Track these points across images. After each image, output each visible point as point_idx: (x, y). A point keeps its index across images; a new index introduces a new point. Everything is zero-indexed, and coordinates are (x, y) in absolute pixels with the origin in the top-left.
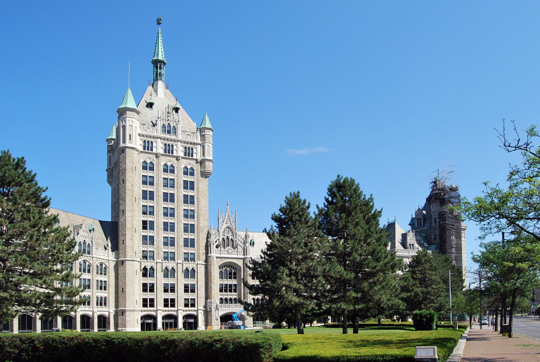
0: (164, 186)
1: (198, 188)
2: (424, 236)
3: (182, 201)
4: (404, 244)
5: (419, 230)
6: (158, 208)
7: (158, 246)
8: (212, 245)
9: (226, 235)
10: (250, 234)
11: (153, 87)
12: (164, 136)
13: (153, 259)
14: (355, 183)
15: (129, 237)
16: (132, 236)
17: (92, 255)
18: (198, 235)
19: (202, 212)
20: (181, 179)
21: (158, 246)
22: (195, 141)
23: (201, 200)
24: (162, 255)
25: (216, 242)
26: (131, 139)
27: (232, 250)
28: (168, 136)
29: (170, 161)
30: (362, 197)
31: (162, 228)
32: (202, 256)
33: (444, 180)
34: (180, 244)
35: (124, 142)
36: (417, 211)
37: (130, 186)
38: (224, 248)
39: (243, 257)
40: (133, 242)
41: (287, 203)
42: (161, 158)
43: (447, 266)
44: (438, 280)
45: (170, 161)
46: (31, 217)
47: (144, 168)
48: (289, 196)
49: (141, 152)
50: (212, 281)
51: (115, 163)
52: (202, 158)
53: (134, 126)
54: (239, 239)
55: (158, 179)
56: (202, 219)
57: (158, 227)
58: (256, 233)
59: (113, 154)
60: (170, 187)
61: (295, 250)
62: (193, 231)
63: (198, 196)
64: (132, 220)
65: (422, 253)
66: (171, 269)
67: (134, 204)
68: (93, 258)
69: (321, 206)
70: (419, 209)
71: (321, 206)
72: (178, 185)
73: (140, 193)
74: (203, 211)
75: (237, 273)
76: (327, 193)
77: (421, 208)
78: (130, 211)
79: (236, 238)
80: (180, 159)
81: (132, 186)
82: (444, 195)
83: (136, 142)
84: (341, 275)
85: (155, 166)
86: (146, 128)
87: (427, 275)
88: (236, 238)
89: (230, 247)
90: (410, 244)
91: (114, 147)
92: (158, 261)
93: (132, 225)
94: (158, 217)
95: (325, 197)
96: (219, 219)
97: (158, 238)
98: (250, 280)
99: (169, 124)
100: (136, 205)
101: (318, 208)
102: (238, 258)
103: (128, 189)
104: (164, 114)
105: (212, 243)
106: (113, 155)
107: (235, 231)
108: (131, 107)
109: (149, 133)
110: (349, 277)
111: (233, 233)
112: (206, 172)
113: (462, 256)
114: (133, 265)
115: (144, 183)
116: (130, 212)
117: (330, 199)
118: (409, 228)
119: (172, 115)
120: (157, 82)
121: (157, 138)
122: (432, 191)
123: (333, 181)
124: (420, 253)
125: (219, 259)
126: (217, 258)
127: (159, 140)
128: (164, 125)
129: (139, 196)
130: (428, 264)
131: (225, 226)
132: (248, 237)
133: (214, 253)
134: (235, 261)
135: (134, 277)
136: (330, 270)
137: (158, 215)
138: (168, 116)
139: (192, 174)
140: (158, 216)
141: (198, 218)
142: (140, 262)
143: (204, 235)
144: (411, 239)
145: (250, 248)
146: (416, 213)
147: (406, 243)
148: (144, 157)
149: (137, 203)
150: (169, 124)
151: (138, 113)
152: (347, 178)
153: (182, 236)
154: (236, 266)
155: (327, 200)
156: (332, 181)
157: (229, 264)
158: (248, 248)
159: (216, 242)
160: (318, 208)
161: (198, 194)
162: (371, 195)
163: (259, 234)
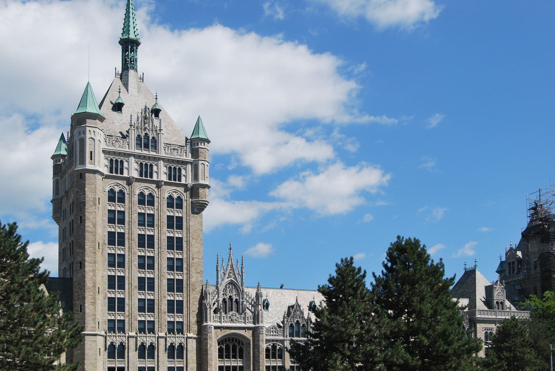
0: (139, 225)
1: (188, 227)
2: (519, 290)
4: (488, 302)
5: (511, 280)
6: (130, 258)
7: (130, 312)
8: (208, 310)
10: (264, 292)
12: (140, 151)
13: (124, 332)
14: (420, 243)
15: (90, 301)
16: (94, 299)
18: (188, 295)
19: (194, 261)
21: (130, 312)
22: (184, 158)
23: (192, 243)
24: (136, 325)
25: (214, 304)
26: (93, 158)
27: (237, 316)
28: (145, 152)
29: (148, 189)
30: (430, 261)
31: (136, 286)
32: (194, 326)
33: (548, 205)
34: (162, 308)
35: (83, 162)
36: (508, 252)
37: (91, 226)
38: (226, 313)
39: (252, 325)
40: (95, 307)
41: (338, 274)
43: (551, 336)
44: (533, 360)
45: (148, 189)
46: (31, 299)
47: (111, 199)
48: (339, 262)
49: (107, 177)
50: (209, 361)
51: (66, 191)
53: (97, 138)
54: (248, 299)
55: (131, 214)
56: (194, 272)
57: (130, 285)
58: (271, 290)
59: (62, 178)
60: (148, 226)
61: (350, 332)
62: (180, 290)
63: (188, 238)
64: (94, 275)
65: (511, 323)
66: (149, 346)
67: (97, 252)
69: (379, 274)
70: (511, 249)
71: (379, 274)
72: (159, 223)
73: (104, 236)
74: (195, 259)
75: (244, 349)
76: (386, 258)
77: (514, 247)
78: (91, 263)
79: (243, 299)
80: (162, 186)
81: (95, 225)
82: (549, 228)
83: (99, 162)
84: (405, 361)
85: (127, 196)
86: (114, 142)
87: (518, 354)
88: (243, 299)
89: (234, 312)
90: (497, 303)
91: (63, 168)
93: (94, 283)
94: (130, 270)
95: (384, 262)
96: (217, 270)
97: (130, 301)
98: (263, 359)
99: (146, 134)
100: (99, 254)
101: (375, 276)
103: (88, 231)
104: (140, 120)
105: (208, 307)
106: (61, 179)
107: (241, 288)
108: (92, 112)
109: (117, 148)
110: (415, 364)
111: (237, 290)
114: (95, 341)
115: (111, 221)
116: (91, 265)
117: (389, 265)
118: (496, 277)
119: (150, 121)
120: (127, 71)
122: (531, 221)
123: (393, 243)
124: (508, 323)
125: (219, 330)
126: (216, 328)
129: (104, 241)
130: (519, 338)
131: (227, 280)
133: (212, 322)
134: (242, 332)
135: (96, 359)
136: (392, 356)
137: (130, 267)
138: (145, 123)
139: (180, 206)
140: (130, 269)
141: (188, 270)
142: (106, 337)
143: (196, 295)
144: (499, 294)
145: (264, 314)
146: (506, 254)
147: (492, 300)
148: (109, 184)
149: (101, 251)
150: (146, 134)
151: (102, 119)
152: (409, 238)
154: (243, 340)
155: (385, 266)
156: (391, 243)
157: (233, 336)
158: (260, 312)
159: (214, 304)
160: (375, 276)
161: (188, 236)
162: (441, 259)
163: (275, 291)
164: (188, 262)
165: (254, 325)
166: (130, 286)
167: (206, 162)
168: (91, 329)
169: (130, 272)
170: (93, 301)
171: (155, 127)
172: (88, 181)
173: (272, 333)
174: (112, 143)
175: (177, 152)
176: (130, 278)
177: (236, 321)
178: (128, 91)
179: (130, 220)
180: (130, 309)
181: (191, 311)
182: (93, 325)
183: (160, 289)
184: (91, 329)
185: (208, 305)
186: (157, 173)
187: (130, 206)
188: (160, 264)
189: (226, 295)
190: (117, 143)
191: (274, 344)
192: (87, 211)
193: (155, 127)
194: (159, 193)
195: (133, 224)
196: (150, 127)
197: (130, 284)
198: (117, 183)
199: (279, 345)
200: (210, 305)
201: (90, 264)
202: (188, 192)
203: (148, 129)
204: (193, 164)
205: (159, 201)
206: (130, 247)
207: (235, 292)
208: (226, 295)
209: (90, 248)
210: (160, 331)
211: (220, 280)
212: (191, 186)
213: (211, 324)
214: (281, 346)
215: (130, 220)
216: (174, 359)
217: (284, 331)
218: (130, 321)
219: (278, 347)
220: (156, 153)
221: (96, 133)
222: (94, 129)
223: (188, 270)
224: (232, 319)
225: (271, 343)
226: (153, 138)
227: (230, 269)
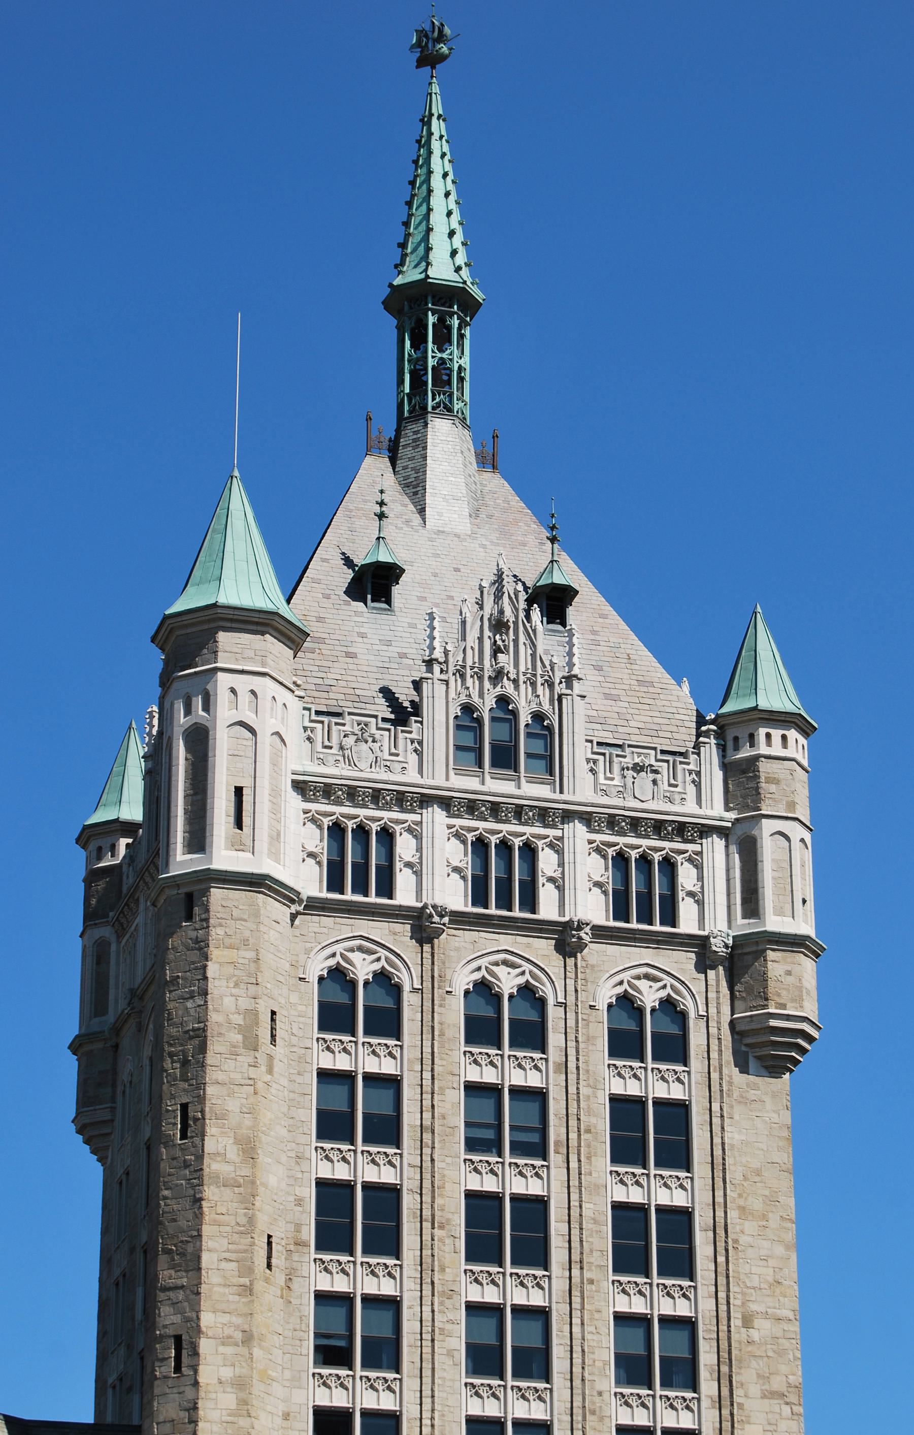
11: (393, 461)
19: (755, 1335)
26: (247, 820)
37: (233, 1153)
49: (315, 906)
52: (744, 926)
74: (757, 1323)
78: (226, 1341)
85: (410, 1002)
86: (351, 740)
94: (427, 1380)
119: (522, 638)
121: (425, 801)
150: (503, 701)
164: (723, 1335)
174: (342, 748)
175: (655, 782)
178: (422, 511)
186: (558, 884)
187: (427, 1049)
188: (577, 1349)
190: (364, 747)
192: (212, 1075)
193: (544, 666)
194: (570, 983)
195: (443, 1141)
196: (522, 668)
198: (362, 937)
201: (222, 1349)
209: (224, 1265)
212: (726, 946)
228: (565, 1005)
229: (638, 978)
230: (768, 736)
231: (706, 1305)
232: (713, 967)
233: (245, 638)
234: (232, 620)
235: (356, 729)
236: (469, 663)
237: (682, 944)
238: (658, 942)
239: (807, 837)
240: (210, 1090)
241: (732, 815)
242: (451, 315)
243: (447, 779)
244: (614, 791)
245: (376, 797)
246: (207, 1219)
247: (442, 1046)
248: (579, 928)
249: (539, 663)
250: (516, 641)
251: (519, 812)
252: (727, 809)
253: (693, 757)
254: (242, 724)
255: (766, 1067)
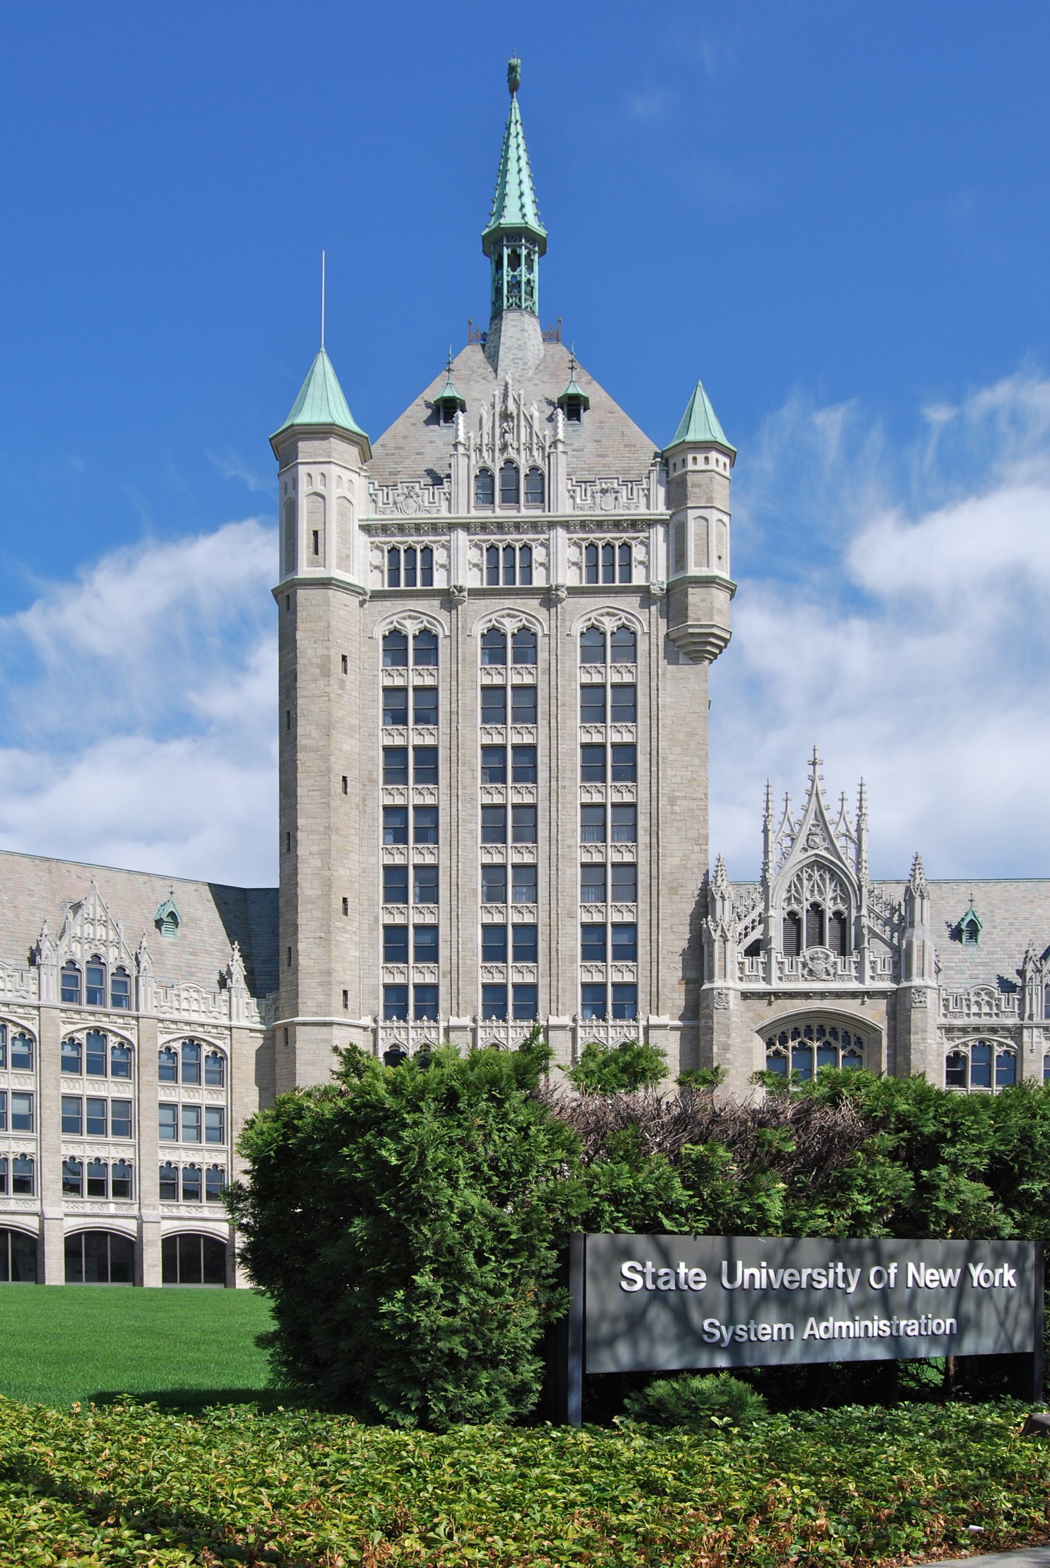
3: (574, 771)
7: (454, 962)
8: (717, 945)
9: (807, 897)
11: (483, 346)
17: (137, 1009)
18: (654, 907)
19: (677, 809)
20: (572, 678)
21: (454, 962)
22: (641, 511)
26: (321, 549)
27: (832, 959)
28: (500, 513)
32: (676, 995)
37: (315, 734)
39: (888, 985)
42: (470, 607)
49: (377, 595)
53: (334, 493)
67: (335, 803)
68: (137, 1018)
72: (553, 708)
74: (678, 803)
85: (443, 645)
86: (402, 498)
88: (859, 908)
92: (454, 1021)
94: (454, 847)
97: (454, 931)
99: (509, 462)
102: (770, 994)
103: (306, 748)
109: (411, 513)
112: (693, 634)
113: (161, 1179)
116: (317, 837)
119: (523, 423)
121: (451, 527)
126: (746, 996)
127: (461, 537)
128: (484, 470)
131: (798, 856)
132: (917, 895)
141: (655, 833)
150: (509, 462)
153: (572, 916)
164: (654, 811)
165: (894, 986)
166: (454, 890)
167: (714, 511)
168: (314, 1010)
169: (454, 853)
170: (323, 935)
171: (538, 437)
172: (304, 614)
173: (975, 1009)
174: (395, 503)
175: (616, 498)
176: (454, 868)
177: (829, 975)
178: (496, 371)
179: (454, 709)
180: (454, 954)
181: (665, 952)
182: (321, 998)
183: (554, 893)
184: (318, 1010)
185: (715, 931)
186: (546, 566)
187: (454, 669)
188: (554, 824)
189: (798, 901)
190: (410, 500)
191: (982, 1042)
192: (300, 693)
193: (538, 437)
194: (553, 622)
195: (464, 718)
196: (523, 440)
197: (455, 886)
198: (410, 610)
199: (1001, 1044)
200: (723, 930)
201: (311, 837)
202: (653, 608)
203: (515, 446)
204: (671, 526)
205: (553, 645)
206: (454, 784)
207: (835, 891)
208: (798, 901)
209: (311, 793)
210: (554, 1012)
211: (774, 857)
212: (662, 590)
213: (725, 985)
214: (1008, 1046)
215: (454, 709)
216: (990, 1086)
217: (1022, 1001)
218: (454, 987)
219: (998, 1051)
220: (544, 511)
221: (333, 481)
222: (324, 468)
223: (654, 836)
224: (810, 970)
225: (972, 1039)
226: (534, 469)
227: (815, 822)
228: (549, 636)
229: (602, 615)
230: (695, 459)
231: (643, 795)
232: (655, 603)
233: (316, 444)
234: (306, 433)
235: (406, 491)
236: (485, 441)
237: (633, 592)
238: (616, 593)
239: (726, 519)
240: (299, 701)
241: (670, 512)
242: (535, 253)
243: (469, 512)
244: (587, 507)
245: (418, 528)
246: (300, 769)
247: (464, 666)
248: (557, 589)
249: (535, 437)
250: (518, 426)
251: (517, 527)
252: (668, 509)
253: (645, 481)
254: (316, 494)
255: (691, 659)
